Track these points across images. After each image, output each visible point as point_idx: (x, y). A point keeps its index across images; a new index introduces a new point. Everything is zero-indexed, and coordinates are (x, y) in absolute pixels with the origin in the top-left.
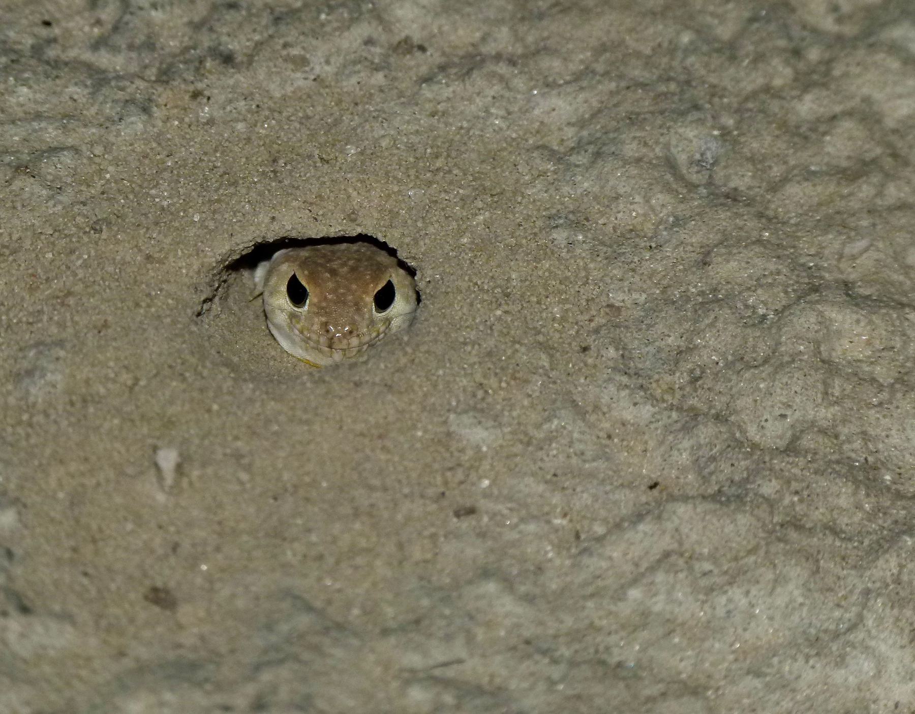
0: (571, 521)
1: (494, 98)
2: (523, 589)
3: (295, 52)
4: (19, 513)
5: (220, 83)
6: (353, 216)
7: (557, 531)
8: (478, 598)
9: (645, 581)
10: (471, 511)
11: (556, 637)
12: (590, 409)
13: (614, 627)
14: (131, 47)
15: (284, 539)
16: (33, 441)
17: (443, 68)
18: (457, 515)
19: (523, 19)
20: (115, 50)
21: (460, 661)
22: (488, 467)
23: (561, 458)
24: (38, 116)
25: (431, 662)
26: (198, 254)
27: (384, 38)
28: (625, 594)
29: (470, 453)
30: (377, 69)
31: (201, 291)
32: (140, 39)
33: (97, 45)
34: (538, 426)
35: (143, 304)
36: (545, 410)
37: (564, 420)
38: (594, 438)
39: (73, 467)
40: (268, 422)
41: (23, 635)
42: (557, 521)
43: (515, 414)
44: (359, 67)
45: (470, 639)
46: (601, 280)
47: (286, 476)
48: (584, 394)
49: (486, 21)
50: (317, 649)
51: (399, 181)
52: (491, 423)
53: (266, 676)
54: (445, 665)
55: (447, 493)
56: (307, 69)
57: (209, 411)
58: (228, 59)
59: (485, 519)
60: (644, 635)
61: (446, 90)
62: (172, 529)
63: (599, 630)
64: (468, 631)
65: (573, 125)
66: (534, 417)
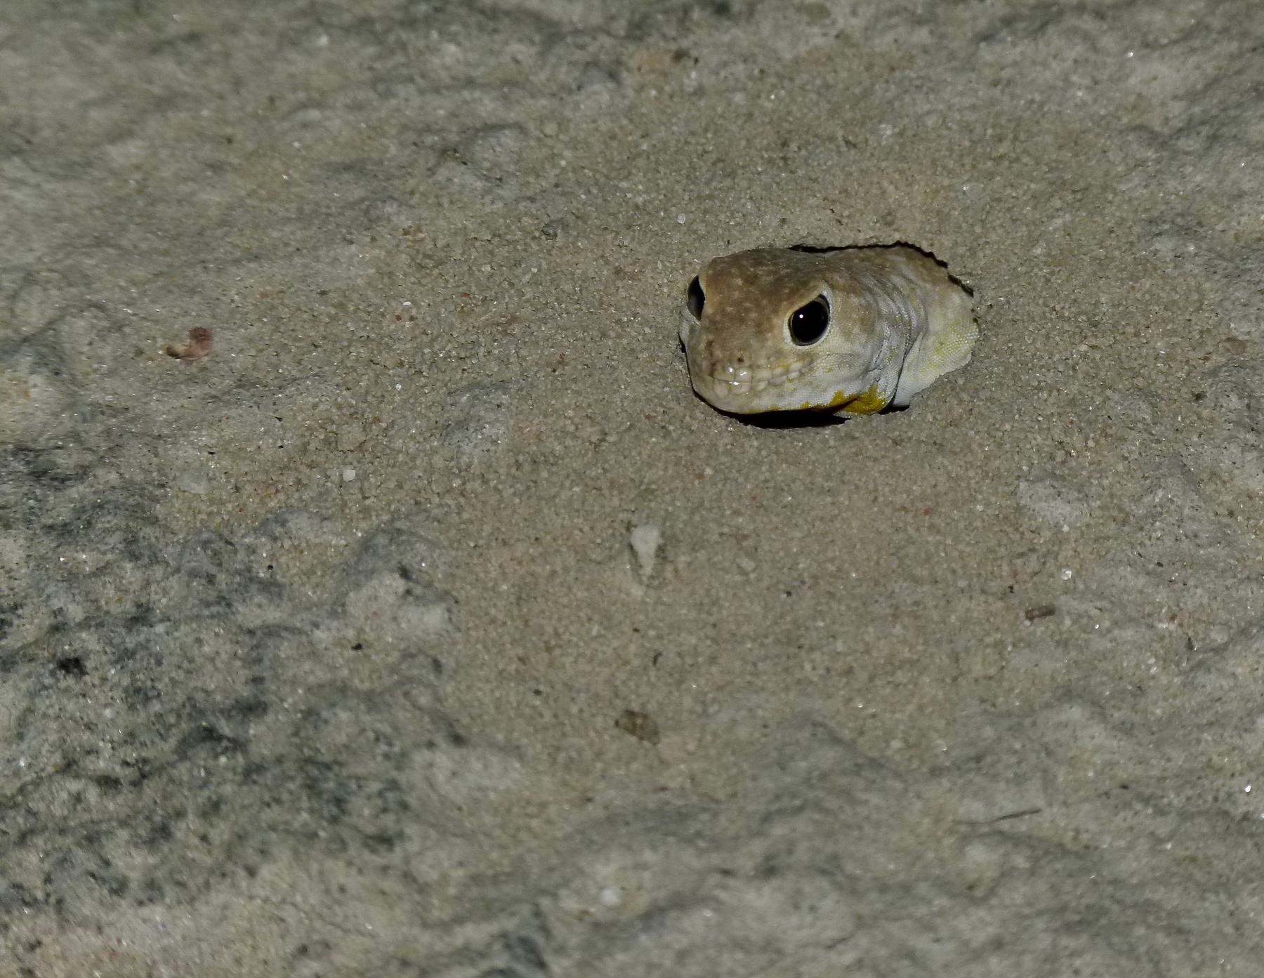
0: (1181, 625)
1: (1076, 61)
4: (449, 611)
8: (1059, 726)
10: (1049, 611)
16: (465, 516)
22: (1071, 553)
23: (1168, 542)
24: (470, 83)
25: (998, 813)
26: (683, 268)
29: (1047, 534)
34: (1137, 499)
35: (613, 334)
36: (1145, 478)
37: (1170, 491)
38: (1211, 514)
40: (779, 491)
43: (1106, 482)
44: (895, 20)
45: (1048, 782)
50: (846, 794)
53: (779, 830)
55: (1016, 587)
56: (827, 21)
57: (700, 476)
59: (1068, 622)
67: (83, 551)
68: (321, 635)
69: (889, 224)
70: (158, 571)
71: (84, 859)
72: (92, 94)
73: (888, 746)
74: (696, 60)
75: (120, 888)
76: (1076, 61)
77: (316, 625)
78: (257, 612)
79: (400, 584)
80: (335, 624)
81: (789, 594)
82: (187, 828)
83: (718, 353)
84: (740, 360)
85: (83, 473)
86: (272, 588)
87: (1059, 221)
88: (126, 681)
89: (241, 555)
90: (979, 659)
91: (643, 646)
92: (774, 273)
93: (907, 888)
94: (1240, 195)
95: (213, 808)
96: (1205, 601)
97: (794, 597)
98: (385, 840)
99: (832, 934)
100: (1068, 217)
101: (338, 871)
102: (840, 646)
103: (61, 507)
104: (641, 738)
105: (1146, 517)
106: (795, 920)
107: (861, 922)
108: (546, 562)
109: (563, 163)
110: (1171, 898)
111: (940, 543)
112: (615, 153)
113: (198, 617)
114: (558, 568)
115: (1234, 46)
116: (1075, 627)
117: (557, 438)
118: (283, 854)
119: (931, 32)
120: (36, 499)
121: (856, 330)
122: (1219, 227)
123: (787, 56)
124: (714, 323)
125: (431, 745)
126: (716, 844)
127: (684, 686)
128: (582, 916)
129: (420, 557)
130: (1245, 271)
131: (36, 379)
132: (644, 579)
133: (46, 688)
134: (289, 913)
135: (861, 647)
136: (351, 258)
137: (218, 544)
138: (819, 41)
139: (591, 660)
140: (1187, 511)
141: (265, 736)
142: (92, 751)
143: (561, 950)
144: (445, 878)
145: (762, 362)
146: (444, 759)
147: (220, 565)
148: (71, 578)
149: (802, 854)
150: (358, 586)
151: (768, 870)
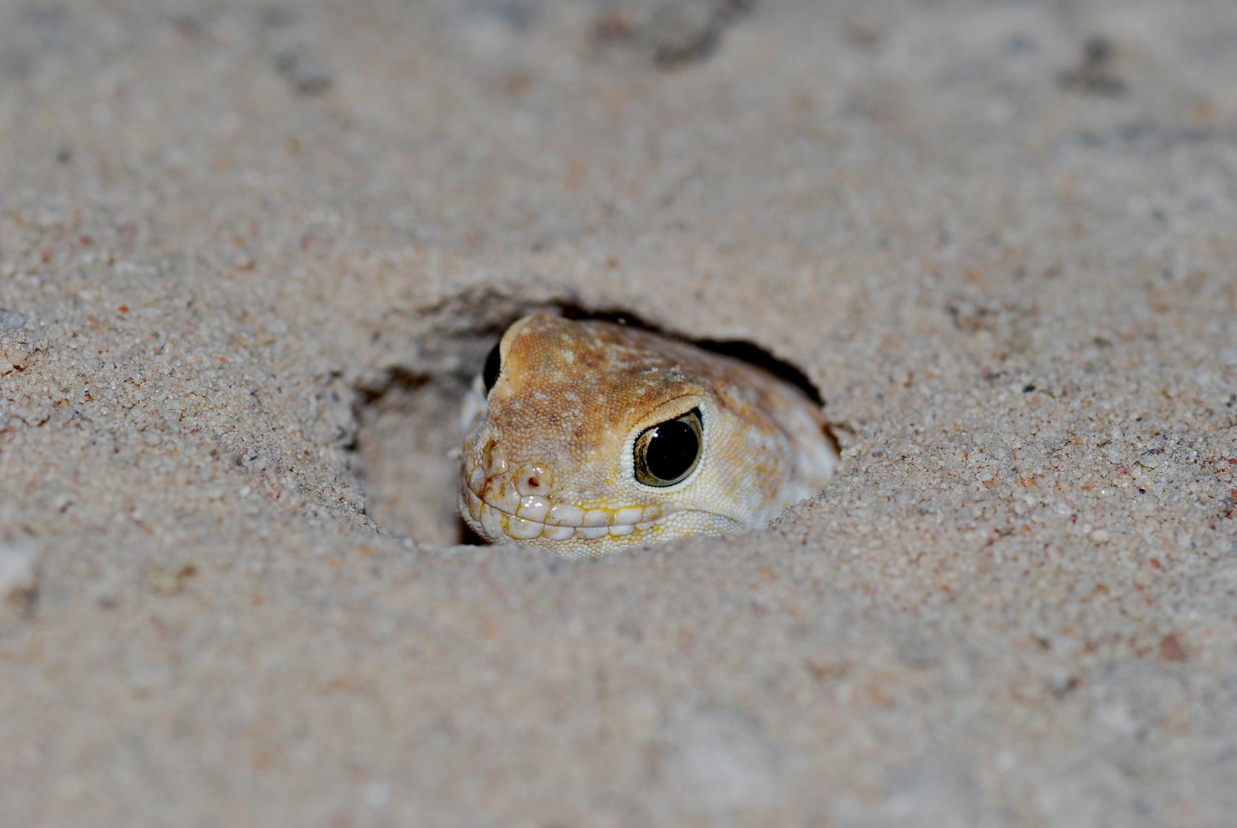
83: (502, 464)
84: (533, 483)
92: (631, 358)
112: (157, 463)
121: (747, 482)
124: (508, 412)
145: (570, 494)
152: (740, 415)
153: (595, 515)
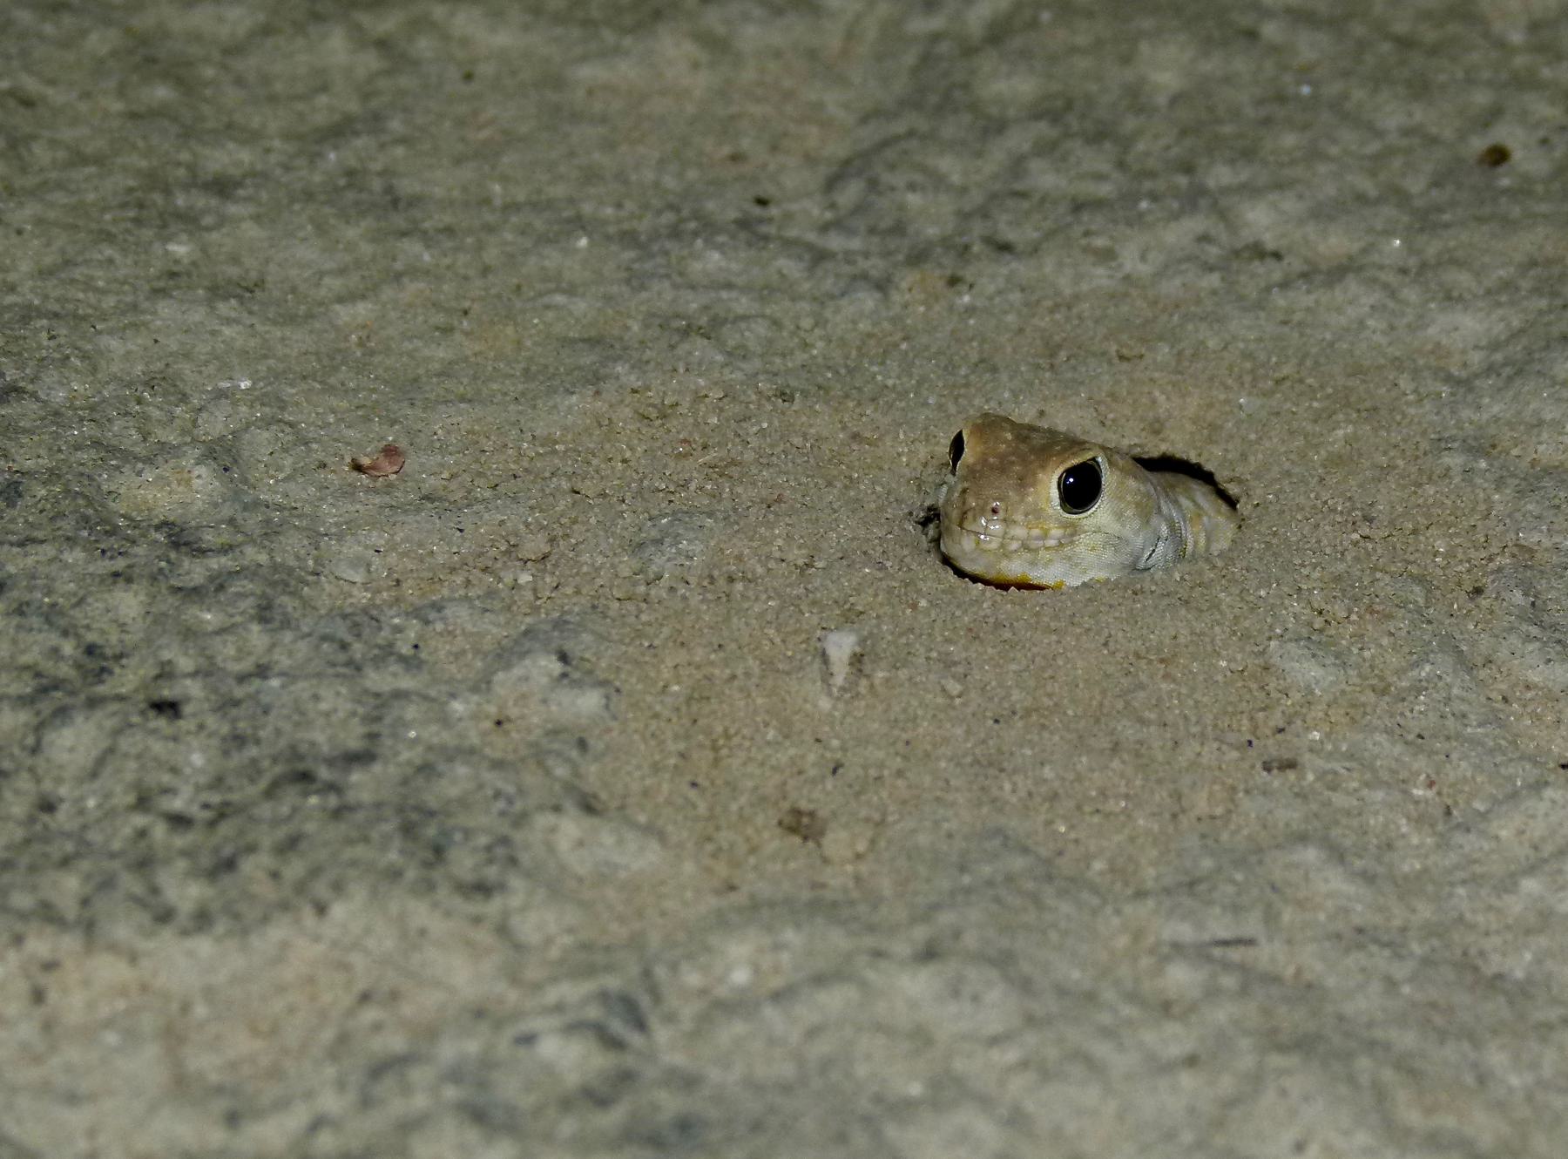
0: (1439, 794)
1: (1372, 307)
2: (1359, 864)
3: (1100, 242)
4: (607, 697)
5: (990, 276)
6: (1157, 426)
7: (1417, 803)
8: (1289, 866)
9: (1547, 868)
10: (1291, 765)
11: (1404, 930)
12: (1479, 661)
13: (1494, 926)
14: (872, 231)
15: (1002, 770)
16: (644, 617)
17: (1304, 276)
18: (1267, 768)
19: (1422, 230)
20: (851, 232)
21: (1250, 942)
22: (1321, 714)
23: (1433, 717)
24: (729, 286)
25: (1206, 937)
26: (927, 441)
27: (1224, 237)
28: (1516, 884)
29: (1296, 696)
30: (1211, 269)
31: (926, 493)
32: (887, 222)
33: (825, 228)
34: (1401, 672)
35: (839, 485)
36: (1411, 653)
37: (1439, 667)
38: (1483, 699)
39: (699, 654)
40: (999, 625)
41: (580, 843)
42: (1418, 792)
43: (1367, 654)
44: (1183, 267)
45: (1271, 917)
46: (1509, 516)
47: (1016, 695)
48: (1473, 644)
49: (1370, 230)
50: (1036, 900)
51: (1227, 388)
52: (1330, 660)
53: (946, 918)
54: (1226, 943)
55: (1255, 742)
56: (1113, 264)
57: (914, 606)
58: (1005, 248)
59: (1310, 777)
60: (1543, 941)
61: (1302, 298)
62: (835, 743)
63: (1472, 927)
64: (1269, 906)
65: (1482, 348)
66: (1394, 660)
67: (209, 610)
68: (458, 707)
69: (1157, 432)
70: (288, 636)
71: (130, 883)
72: (330, 265)
73: (1088, 867)
74: (971, 286)
75: (165, 916)
76: (1372, 307)
77: (453, 696)
78: (380, 680)
79: (557, 667)
80: (475, 698)
81: (996, 721)
82: (253, 867)
85: (226, 549)
86: (411, 663)
87: (1340, 433)
88: (225, 729)
89: (385, 633)
90: (1204, 795)
91: (822, 756)
93: (1091, 997)
94: (1540, 423)
95: (291, 844)
96: (1469, 774)
97: (1002, 724)
98: (482, 889)
99: (995, 1027)
100: (1350, 429)
101: (421, 913)
102: (1048, 772)
103: (195, 571)
104: (805, 838)
105: (1410, 689)
106: (952, 1008)
107: (1030, 1020)
108: (727, 665)
109: (815, 352)
110: (1407, 1040)
111: (1173, 690)
113: (319, 675)
114: (739, 672)
115: (1543, 303)
116: (1318, 785)
117: (760, 561)
118: (359, 893)
119: (1223, 279)
120: (168, 562)
121: (1129, 513)
122: (1515, 452)
123: (1068, 291)
125: (557, 809)
126: (871, 928)
127: (863, 798)
128: (703, 992)
129: (582, 645)
130: (1539, 489)
131: (202, 470)
132: (835, 690)
133: (131, 726)
134: (357, 959)
135: (1071, 776)
136: (570, 408)
137: (363, 620)
138: (1105, 282)
139: (762, 764)
140: (1455, 691)
141: (362, 784)
142: (168, 791)
143: (670, 1018)
144: (549, 941)
145: (1019, 517)
146: (570, 827)
147: (358, 635)
148: (189, 634)
149: (970, 940)
150: (508, 666)
151: (929, 954)
152: (1122, 470)
153: (1036, 532)
